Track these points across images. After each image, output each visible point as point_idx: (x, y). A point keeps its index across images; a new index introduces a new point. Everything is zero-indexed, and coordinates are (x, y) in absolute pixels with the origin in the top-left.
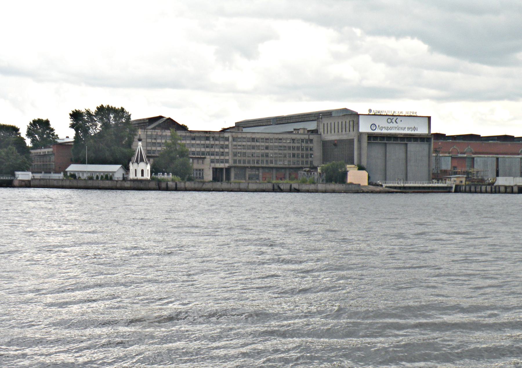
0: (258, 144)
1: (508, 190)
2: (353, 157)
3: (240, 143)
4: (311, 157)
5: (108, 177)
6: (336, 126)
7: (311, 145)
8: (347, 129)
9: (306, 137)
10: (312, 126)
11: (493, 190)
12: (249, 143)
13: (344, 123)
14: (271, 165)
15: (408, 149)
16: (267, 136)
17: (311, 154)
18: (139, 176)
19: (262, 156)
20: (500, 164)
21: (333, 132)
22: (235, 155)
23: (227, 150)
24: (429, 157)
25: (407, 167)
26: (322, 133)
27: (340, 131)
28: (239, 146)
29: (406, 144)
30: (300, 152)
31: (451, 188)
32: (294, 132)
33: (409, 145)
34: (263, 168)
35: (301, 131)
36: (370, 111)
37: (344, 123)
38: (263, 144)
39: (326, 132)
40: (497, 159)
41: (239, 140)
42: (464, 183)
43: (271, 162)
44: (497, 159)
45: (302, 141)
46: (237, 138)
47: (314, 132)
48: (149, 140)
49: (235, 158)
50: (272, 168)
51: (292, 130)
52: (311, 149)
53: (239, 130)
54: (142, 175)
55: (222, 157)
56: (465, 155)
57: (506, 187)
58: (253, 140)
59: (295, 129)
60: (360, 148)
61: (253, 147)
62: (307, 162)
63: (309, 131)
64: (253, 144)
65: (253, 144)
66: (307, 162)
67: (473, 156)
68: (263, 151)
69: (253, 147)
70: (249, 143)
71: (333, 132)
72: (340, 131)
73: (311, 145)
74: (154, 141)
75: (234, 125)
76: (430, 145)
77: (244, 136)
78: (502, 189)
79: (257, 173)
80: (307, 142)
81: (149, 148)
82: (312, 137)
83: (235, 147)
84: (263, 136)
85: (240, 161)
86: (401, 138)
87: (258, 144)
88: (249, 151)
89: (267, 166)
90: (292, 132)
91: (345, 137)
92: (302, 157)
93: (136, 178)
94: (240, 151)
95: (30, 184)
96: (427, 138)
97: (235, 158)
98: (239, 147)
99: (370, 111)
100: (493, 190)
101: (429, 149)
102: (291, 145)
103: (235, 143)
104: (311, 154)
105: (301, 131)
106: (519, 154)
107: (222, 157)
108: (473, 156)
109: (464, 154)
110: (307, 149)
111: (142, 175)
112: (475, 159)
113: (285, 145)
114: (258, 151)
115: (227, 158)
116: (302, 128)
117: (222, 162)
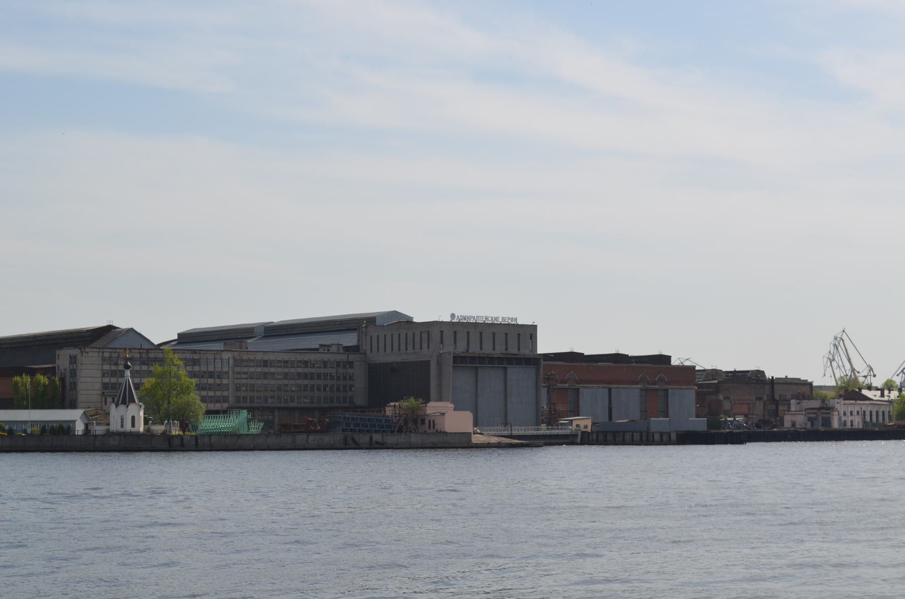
0: (272, 370)
1: (665, 438)
2: (429, 389)
3: (245, 370)
4: (350, 390)
5: (65, 429)
6: (389, 342)
7: (351, 371)
8: (417, 346)
9: (344, 357)
10: (350, 339)
11: (644, 438)
12: (259, 369)
13: (410, 336)
14: (292, 405)
15: (508, 377)
16: (286, 357)
17: (352, 386)
18: (128, 427)
19: (279, 389)
20: (613, 398)
21: (389, 349)
22: (238, 389)
23: (225, 381)
24: (537, 390)
25: (506, 405)
26: (368, 352)
27: (403, 347)
28: (244, 373)
29: (505, 368)
30: (329, 382)
31: (576, 435)
32: (321, 350)
33: (509, 370)
34: (280, 409)
35: (334, 349)
36: (453, 316)
37: (410, 336)
38: (280, 370)
39: (375, 349)
40: (610, 390)
41: (244, 364)
42: (589, 430)
43: (292, 400)
44: (610, 390)
45: (338, 364)
46: (242, 360)
47: (355, 349)
48: (106, 367)
49: (238, 394)
50: (293, 409)
51: (318, 346)
52: (351, 378)
53: (241, 348)
54: (133, 425)
55: (218, 393)
56: (657, 386)
57: (661, 434)
58: (265, 363)
59: (321, 346)
60: (440, 376)
61: (265, 375)
62: (345, 398)
63: (344, 347)
64: (266, 370)
65: (266, 370)
66: (345, 398)
67: (578, 386)
68: (280, 382)
69: (265, 375)
70: (259, 369)
71: (389, 349)
72: (403, 347)
73: (351, 371)
74: (113, 368)
75: (176, 337)
76: (538, 370)
77: (252, 357)
78: (657, 437)
79: (271, 417)
80: (344, 367)
81: (106, 380)
82: (352, 357)
83: (238, 376)
84: (281, 357)
85: (245, 398)
86: (498, 358)
87: (272, 370)
88: (259, 382)
89: (286, 405)
90: (317, 349)
91: (413, 358)
92: (338, 390)
93: (122, 430)
94: (245, 381)
95: (827, 422)
96: (480, 358)
97: (238, 394)
98: (244, 376)
99: (453, 316)
100: (644, 438)
101: (537, 376)
102: (322, 371)
103: (238, 369)
104: (352, 386)
105: (334, 349)
106: (637, 384)
107: (218, 393)
108: (578, 386)
109: (565, 383)
110: (345, 378)
111: (133, 425)
112: (670, 391)
113: (313, 370)
114: (273, 382)
115: (225, 393)
116: (335, 342)
117: (218, 401)
